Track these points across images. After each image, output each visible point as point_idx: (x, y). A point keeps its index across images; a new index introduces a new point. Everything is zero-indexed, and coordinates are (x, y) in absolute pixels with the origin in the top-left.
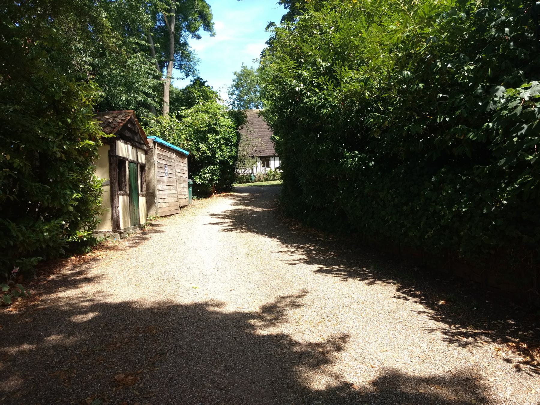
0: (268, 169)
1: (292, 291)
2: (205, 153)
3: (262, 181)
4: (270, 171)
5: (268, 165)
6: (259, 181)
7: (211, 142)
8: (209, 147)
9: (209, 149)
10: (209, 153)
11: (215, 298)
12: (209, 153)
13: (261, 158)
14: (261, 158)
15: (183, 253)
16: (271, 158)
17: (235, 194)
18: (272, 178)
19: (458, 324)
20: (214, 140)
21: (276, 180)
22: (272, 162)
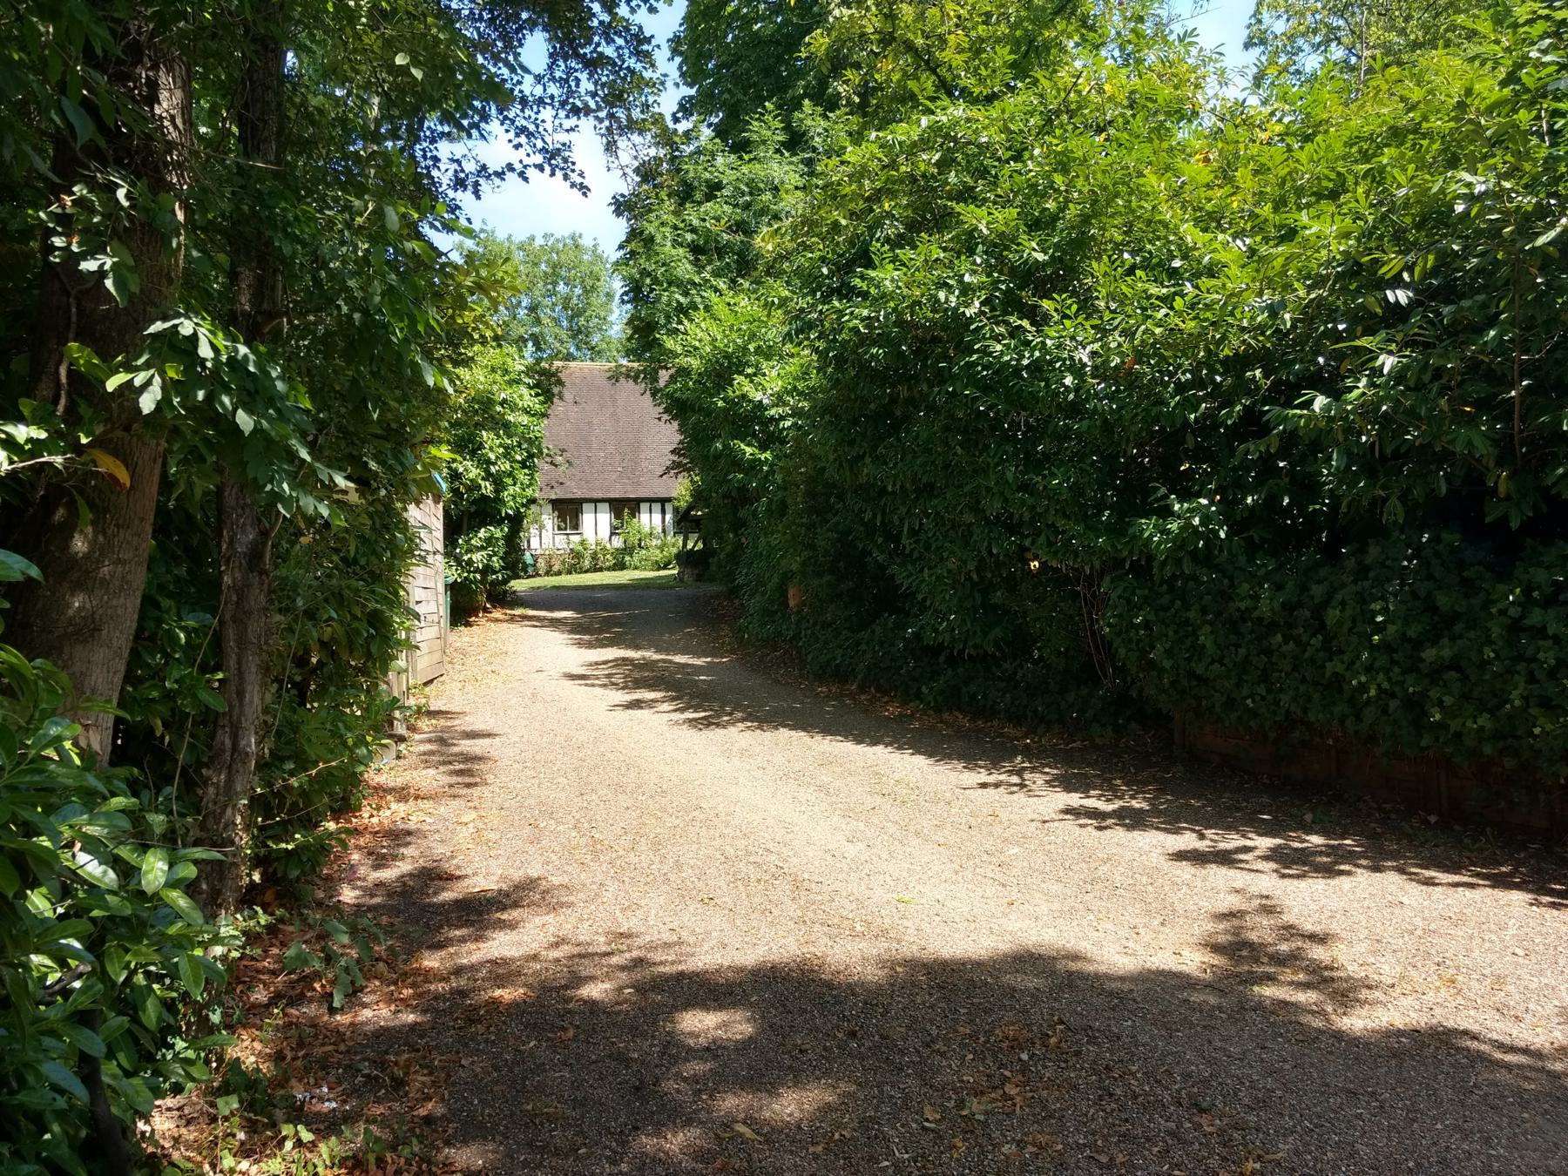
0: (576, 539)
1: (1098, 944)
2: (475, 486)
3: (559, 573)
4: (582, 543)
5: (576, 526)
6: (548, 573)
7: (492, 456)
8: (487, 471)
9: (488, 476)
10: (487, 488)
11: (1148, 965)
12: (487, 488)
13: (557, 504)
14: (557, 504)
15: (608, 807)
16: (585, 506)
17: (531, 613)
18: (587, 564)
19: (592, 1005)
20: (501, 450)
21: (601, 570)
22: (587, 518)
